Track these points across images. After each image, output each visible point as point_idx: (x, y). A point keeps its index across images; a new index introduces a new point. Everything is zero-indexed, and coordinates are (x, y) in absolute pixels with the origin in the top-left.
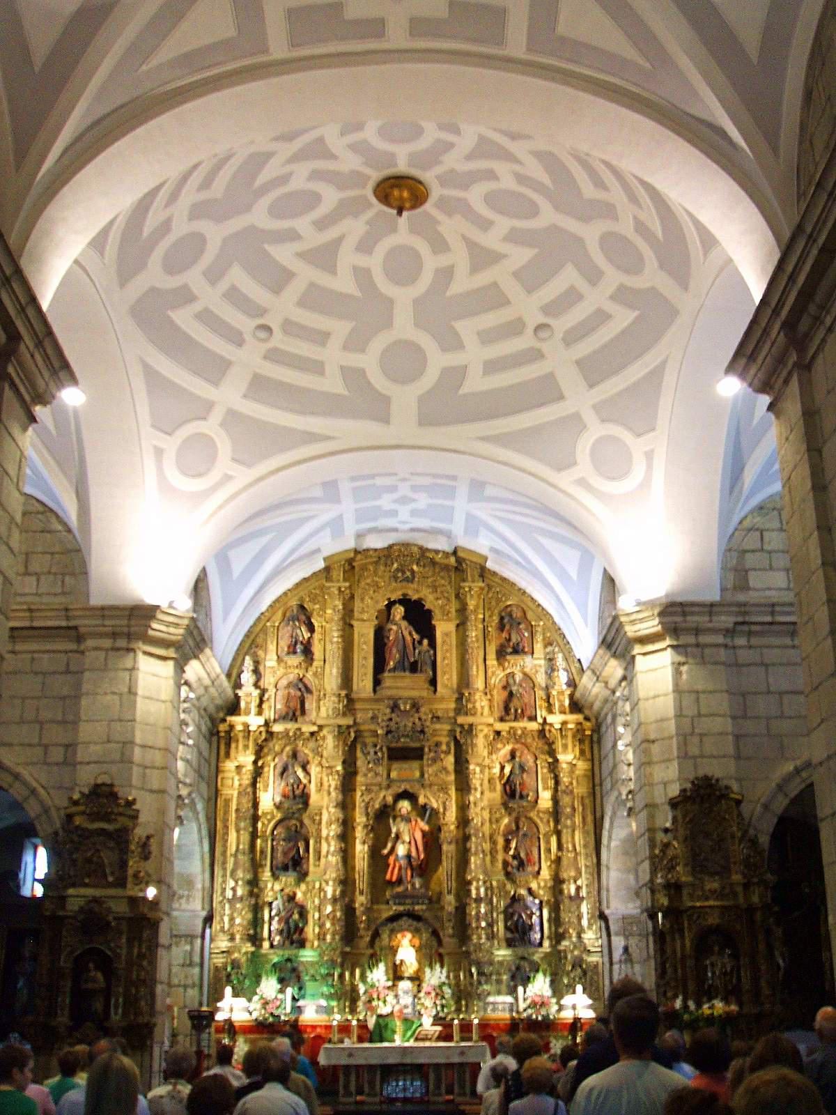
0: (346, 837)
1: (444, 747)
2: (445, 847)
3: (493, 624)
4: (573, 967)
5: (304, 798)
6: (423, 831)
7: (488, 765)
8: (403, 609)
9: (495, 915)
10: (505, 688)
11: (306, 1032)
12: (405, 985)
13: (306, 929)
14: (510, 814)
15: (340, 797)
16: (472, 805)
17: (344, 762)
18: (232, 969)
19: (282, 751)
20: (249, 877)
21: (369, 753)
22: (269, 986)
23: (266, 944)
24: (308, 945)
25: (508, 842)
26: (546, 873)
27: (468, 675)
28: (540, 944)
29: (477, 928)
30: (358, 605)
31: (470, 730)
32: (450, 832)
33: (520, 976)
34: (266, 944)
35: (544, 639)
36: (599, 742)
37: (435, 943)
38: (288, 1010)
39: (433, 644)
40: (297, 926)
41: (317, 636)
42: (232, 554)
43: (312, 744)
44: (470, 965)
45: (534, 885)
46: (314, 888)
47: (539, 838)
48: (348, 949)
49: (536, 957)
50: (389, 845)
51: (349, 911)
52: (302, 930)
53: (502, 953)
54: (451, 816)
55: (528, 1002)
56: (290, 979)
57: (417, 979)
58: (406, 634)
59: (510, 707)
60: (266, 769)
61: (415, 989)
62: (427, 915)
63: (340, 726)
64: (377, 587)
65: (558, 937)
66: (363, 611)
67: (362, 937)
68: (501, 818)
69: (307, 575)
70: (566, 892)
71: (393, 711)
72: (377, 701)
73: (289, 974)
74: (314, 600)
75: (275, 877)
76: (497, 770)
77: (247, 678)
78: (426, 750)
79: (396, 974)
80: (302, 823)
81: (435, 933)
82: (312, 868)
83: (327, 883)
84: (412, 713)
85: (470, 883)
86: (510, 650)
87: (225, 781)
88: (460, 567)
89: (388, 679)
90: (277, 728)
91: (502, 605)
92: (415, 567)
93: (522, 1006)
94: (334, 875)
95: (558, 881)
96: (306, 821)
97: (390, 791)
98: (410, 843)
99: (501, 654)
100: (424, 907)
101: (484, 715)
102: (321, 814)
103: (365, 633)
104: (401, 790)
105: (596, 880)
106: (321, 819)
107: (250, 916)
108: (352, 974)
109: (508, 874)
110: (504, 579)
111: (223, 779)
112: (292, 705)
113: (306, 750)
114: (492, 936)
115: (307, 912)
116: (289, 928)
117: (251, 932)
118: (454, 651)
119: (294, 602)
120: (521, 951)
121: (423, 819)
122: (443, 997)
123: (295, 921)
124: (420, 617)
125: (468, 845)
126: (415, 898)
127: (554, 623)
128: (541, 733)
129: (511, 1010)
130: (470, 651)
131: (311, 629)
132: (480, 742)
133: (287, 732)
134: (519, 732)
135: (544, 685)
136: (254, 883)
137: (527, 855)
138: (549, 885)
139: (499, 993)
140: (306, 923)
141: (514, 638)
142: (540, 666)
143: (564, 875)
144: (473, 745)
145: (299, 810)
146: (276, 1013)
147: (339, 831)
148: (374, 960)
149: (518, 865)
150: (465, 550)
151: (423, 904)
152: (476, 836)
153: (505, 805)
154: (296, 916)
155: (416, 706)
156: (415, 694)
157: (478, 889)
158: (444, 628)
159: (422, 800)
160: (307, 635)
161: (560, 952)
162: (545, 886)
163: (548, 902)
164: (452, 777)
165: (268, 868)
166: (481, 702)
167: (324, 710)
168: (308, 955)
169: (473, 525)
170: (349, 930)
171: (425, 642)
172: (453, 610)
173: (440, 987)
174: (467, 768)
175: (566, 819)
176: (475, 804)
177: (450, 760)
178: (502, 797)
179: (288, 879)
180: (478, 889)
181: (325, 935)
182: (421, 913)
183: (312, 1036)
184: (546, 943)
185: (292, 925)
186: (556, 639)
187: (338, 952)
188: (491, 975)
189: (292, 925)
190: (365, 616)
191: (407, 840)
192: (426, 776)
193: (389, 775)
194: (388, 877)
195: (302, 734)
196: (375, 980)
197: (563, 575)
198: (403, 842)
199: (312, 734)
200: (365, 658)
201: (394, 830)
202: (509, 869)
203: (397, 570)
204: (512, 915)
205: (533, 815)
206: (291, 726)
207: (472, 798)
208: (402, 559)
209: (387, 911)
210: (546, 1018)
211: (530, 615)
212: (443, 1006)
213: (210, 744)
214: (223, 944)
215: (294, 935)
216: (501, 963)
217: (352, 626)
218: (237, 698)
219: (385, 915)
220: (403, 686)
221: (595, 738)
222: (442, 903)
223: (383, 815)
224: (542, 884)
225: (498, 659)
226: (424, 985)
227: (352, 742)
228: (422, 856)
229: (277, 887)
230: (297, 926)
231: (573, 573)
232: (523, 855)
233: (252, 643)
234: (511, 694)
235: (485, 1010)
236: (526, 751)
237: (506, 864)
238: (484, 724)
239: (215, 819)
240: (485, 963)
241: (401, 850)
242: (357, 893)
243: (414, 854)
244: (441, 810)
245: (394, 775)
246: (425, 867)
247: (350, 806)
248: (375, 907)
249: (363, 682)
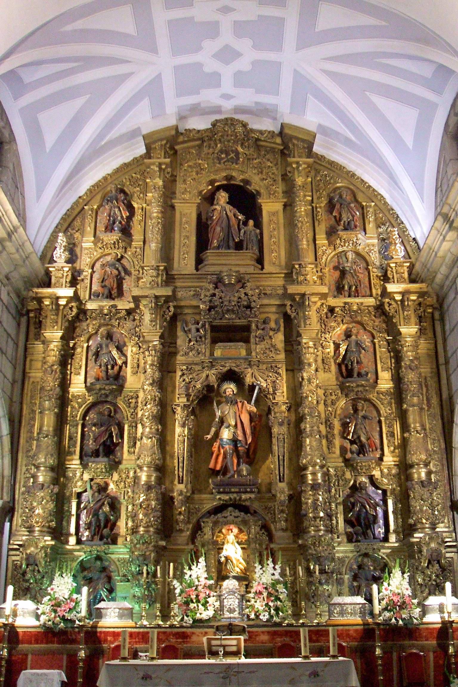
0: (163, 417)
1: (273, 325)
2: (275, 430)
3: (323, 205)
4: (429, 562)
5: (117, 379)
6: (250, 413)
7: (321, 343)
8: (227, 195)
9: (333, 506)
10: (336, 268)
11: (106, 641)
12: (230, 584)
13: (118, 523)
14: (347, 396)
15: (157, 375)
16: (305, 382)
17: (162, 337)
18: (27, 566)
19: (96, 333)
20: (51, 461)
21: (190, 330)
22: (62, 585)
23: (72, 540)
24: (120, 540)
25: (345, 425)
26: (389, 459)
27: (298, 250)
28: (386, 539)
29: (315, 518)
30: (180, 186)
31: (300, 302)
32: (281, 412)
33: (366, 575)
34: (72, 540)
35: (376, 220)
36: (442, 320)
37: (265, 538)
38: (84, 613)
39: (258, 225)
40: (107, 520)
41: (138, 217)
42: (43, 117)
43: (129, 324)
44: (308, 561)
45: (376, 473)
46: (128, 477)
47: (380, 422)
48: (163, 543)
49: (384, 552)
50: (213, 430)
51: (167, 502)
52: (114, 525)
53: (343, 550)
54: (282, 396)
55: (384, 603)
56: (98, 579)
57: (245, 579)
58: (231, 215)
59: (343, 282)
60: (79, 350)
61: (243, 589)
62: (256, 506)
63: (156, 297)
64: (200, 170)
65: (407, 530)
66: (185, 191)
67: (181, 531)
68: (338, 399)
69: (127, 161)
70: (416, 476)
71: (216, 287)
72: (200, 278)
73: (97, 577)
74: (134, 182)
75: (85, 466)
76: (331, 349)
77: (60, 255)
78: (253, 326)
79: (220, 573)
80: (117, 409)
81: (265, 527)
82: (126, 455)
83: (141, 468)
84: (237, 287)
85: (305, 468)
86: (341, 227)
87: (33, 363)
88: (288, 146)
89: (210, 256)
90: (91, 306)
91: (331, 187)
92: (240, 149)
93: (377, 608)
94: (148, 459)
95: (405, 468)
96: (121, 404)
97: (213, 371)
98: (236, 426)
99: (331, 233)
100: (253, 496)
101: (315, 284)
102: (137, 397)
103: (187, 211)
104: (225, 369)
105: (446, 468)
106: (137, 402)
107: (51, 506)
108: (165, 572)
109: (347, 462)
110: (332, 163)
111: (31, 360)
112: (107, 283)
113: (122, 331)
114: (331, 530)
115: (120, 503)
116: (98, 520)
117: (53, 524)
118: (282, 230)
119: (111, 188)
120: (364, 546)
121: (249, 402)
122: (278, 599)
123: (104, 513)
124: (245, 200)
125: (303, 426)
126: (243, 487)
127: (386, 203)
128: (380, 309)
129: (363, 614)
130: (299, 225)
131: (130, 208)
132: (313, 314)
133: (101, 309)
134: (355, 308)
135: (378, 264)
136: (59, 471)
137: (368, 439)
138: (394, 471)
139: (340, 594)
140: (118, 518)
141: (345, 218)
142: (373, 245)
143: (414, 459)
144: (306, 318)
145: (112, 391)
146: (68, 616)
147: (155, 410)
148: (195, 557)
149: (360, 448)
150: (291, 127)
151: (251, 492)
152: (310, 415)
153: (342, 387)
154: (106, 508)
155: (241, 281)
156: (242, 270)
157: (314, 474)
158: (270, 207)
159: (249, 380)
160: (126, 214)
161: (412, 544)
162: (389, 474)
163: (393, 491)
164: (282, 356)
165: (77, 456)
166: (311, 273)
167: (143, 284)
168: (120, 552)
169: (303, 87)
170: (166, 526)
171: (251, 222)
172: (280, 190)
173: (273, 585)
174: (299, 343)
175: (413, 396)
176: (309, 381)
177: (279, 339)
178: (337, 379)
179: (99, 465)
180: (314, 474)
181: (137, 527)
182: (248, 503)
183: (113, 646)
184: (393, 538)
185: (102, 518)
186: (389, 218)
187: (151, 548)
188: (332, 573)
189: (102, 518)
190: (187, 196)
191: (232, 423)
192: (254, 354)
193: (212, 354)
194: (211, 465)
195: (118, 311)
196: (194, 577)
197: (397, 143)
198: (228, 427)
199: (129, 312)
200: (187, 237)
201: (218, 414)
202: (349, 455)
203: (221, 151)
204: (353, 505)
205: (372, 396)
206: (106, 304)
207: (305, 375)
208: (228, 136)
209: (209, 501)
210: (408, 622)
211: (360, 197)
212: (277, 609)
213: (19, 325)
214: (22, 537)
215: (104, 529)
216: (341, 561)
217: (173, 207)
218: (48, 274)
219: (208, 506)
220: (226, 263)
221: (437, 315)
222: (273, 492)
223: (205, 400)
224: (386, 471)
225: (328, 239)
226: (255, 584)
227: (172, 323)
228: (249, 441)
229: (86, 477)
230: (107, 520)
231: (409, 142)
232: (363, 439)
233: (69, 225)
234: (343, 273)
235: (330, 613)
236: (362, 331)
237: (343, 450)
238: (317, 294)
239: (21, 403)
240: (326, 558)
241: (226, 434)
242: (176, 482)
243: (240, 437)
244: (271, 390)
245: (218, 353)
246: (252, 453)
247: (170, 389)
248: (196, 496)
249: (185, 260)
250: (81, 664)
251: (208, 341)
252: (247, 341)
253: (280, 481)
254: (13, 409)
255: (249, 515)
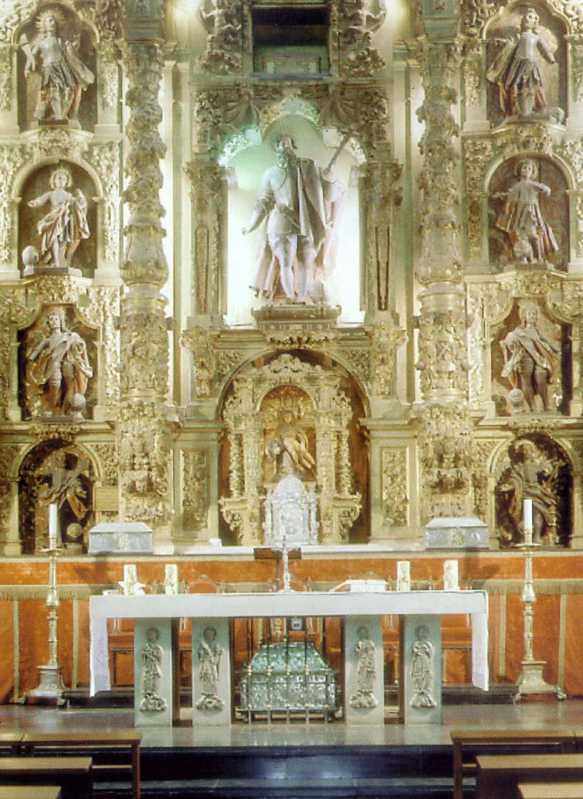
250: (529, 609)
251: (250, 43)
252: (322, 41)
253: (380, 308)
254: (550, 305)
255: (318, 367)
